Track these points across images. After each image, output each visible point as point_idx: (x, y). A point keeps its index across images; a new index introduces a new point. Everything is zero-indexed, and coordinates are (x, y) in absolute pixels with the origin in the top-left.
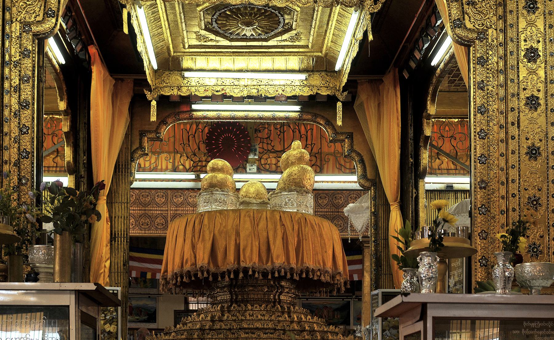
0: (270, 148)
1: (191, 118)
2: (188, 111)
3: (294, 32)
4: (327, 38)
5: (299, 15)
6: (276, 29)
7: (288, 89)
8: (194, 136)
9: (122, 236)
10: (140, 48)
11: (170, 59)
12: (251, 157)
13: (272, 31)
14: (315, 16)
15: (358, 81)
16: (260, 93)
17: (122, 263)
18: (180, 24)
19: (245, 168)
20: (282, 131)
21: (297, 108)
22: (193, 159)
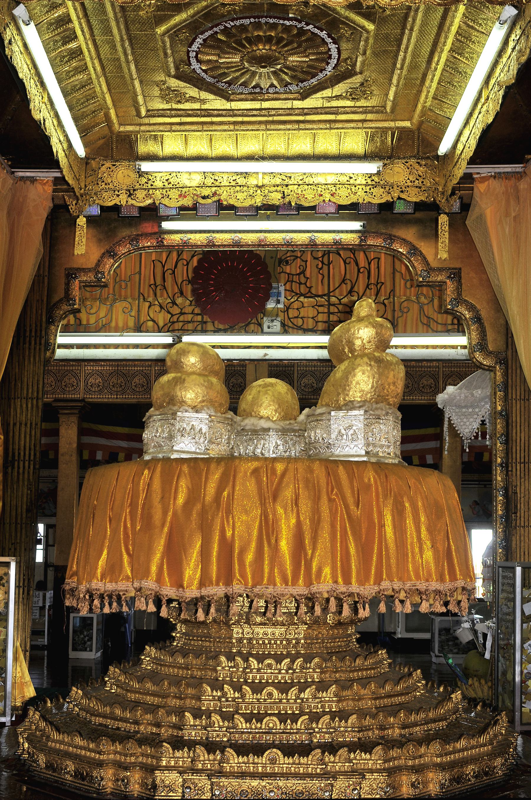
0: (303, 289)
1: (160, 245)
2: (155, 233)
3: (357, 79)
4: (425, 90)
5: (371, 41)
6: (321, 71)
7: (343, 192)
8: (174, 272)
9: (27, 458)
10: (39, 111)
11: (114, 137)
12: (270, 305)
13: (313, 76)
14: (405, 41)
15: (475, 176)
16: (287, 200)
17: (25, 507)
18: (124, 65)
19: (260, 325)
20: (326, 261)
21: (357, 225)
22: (171, 310)
